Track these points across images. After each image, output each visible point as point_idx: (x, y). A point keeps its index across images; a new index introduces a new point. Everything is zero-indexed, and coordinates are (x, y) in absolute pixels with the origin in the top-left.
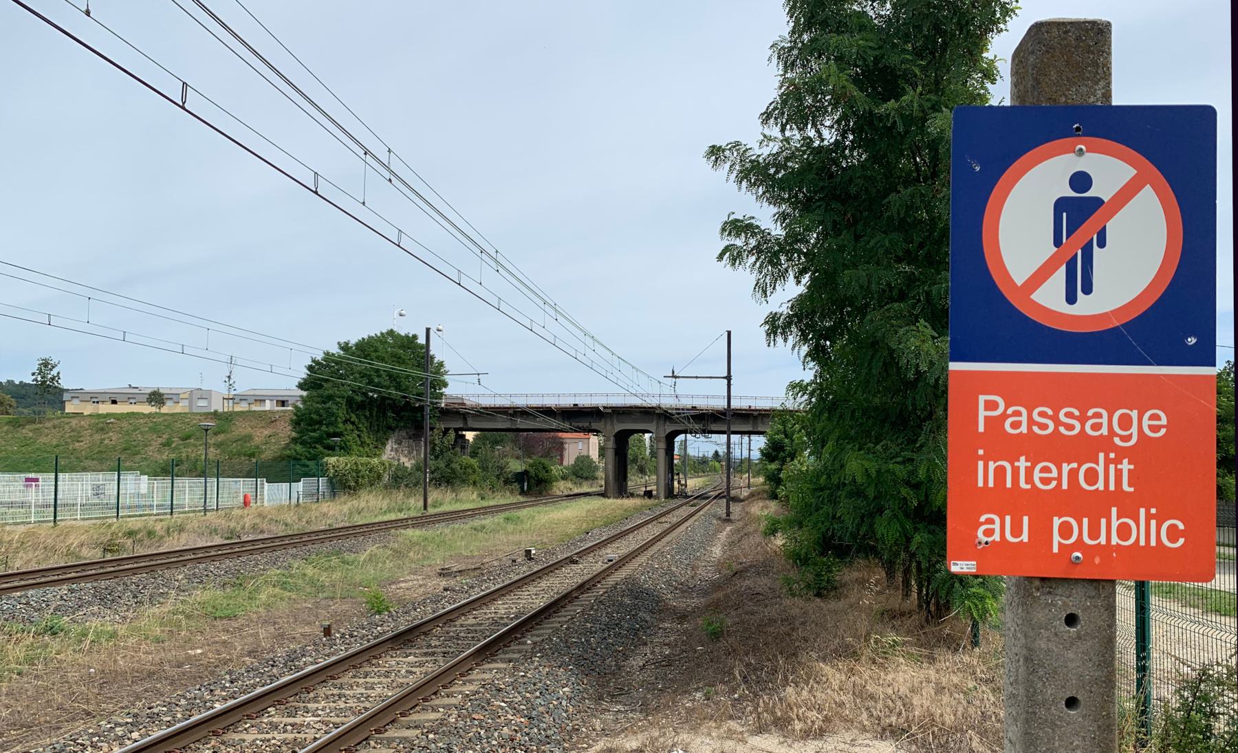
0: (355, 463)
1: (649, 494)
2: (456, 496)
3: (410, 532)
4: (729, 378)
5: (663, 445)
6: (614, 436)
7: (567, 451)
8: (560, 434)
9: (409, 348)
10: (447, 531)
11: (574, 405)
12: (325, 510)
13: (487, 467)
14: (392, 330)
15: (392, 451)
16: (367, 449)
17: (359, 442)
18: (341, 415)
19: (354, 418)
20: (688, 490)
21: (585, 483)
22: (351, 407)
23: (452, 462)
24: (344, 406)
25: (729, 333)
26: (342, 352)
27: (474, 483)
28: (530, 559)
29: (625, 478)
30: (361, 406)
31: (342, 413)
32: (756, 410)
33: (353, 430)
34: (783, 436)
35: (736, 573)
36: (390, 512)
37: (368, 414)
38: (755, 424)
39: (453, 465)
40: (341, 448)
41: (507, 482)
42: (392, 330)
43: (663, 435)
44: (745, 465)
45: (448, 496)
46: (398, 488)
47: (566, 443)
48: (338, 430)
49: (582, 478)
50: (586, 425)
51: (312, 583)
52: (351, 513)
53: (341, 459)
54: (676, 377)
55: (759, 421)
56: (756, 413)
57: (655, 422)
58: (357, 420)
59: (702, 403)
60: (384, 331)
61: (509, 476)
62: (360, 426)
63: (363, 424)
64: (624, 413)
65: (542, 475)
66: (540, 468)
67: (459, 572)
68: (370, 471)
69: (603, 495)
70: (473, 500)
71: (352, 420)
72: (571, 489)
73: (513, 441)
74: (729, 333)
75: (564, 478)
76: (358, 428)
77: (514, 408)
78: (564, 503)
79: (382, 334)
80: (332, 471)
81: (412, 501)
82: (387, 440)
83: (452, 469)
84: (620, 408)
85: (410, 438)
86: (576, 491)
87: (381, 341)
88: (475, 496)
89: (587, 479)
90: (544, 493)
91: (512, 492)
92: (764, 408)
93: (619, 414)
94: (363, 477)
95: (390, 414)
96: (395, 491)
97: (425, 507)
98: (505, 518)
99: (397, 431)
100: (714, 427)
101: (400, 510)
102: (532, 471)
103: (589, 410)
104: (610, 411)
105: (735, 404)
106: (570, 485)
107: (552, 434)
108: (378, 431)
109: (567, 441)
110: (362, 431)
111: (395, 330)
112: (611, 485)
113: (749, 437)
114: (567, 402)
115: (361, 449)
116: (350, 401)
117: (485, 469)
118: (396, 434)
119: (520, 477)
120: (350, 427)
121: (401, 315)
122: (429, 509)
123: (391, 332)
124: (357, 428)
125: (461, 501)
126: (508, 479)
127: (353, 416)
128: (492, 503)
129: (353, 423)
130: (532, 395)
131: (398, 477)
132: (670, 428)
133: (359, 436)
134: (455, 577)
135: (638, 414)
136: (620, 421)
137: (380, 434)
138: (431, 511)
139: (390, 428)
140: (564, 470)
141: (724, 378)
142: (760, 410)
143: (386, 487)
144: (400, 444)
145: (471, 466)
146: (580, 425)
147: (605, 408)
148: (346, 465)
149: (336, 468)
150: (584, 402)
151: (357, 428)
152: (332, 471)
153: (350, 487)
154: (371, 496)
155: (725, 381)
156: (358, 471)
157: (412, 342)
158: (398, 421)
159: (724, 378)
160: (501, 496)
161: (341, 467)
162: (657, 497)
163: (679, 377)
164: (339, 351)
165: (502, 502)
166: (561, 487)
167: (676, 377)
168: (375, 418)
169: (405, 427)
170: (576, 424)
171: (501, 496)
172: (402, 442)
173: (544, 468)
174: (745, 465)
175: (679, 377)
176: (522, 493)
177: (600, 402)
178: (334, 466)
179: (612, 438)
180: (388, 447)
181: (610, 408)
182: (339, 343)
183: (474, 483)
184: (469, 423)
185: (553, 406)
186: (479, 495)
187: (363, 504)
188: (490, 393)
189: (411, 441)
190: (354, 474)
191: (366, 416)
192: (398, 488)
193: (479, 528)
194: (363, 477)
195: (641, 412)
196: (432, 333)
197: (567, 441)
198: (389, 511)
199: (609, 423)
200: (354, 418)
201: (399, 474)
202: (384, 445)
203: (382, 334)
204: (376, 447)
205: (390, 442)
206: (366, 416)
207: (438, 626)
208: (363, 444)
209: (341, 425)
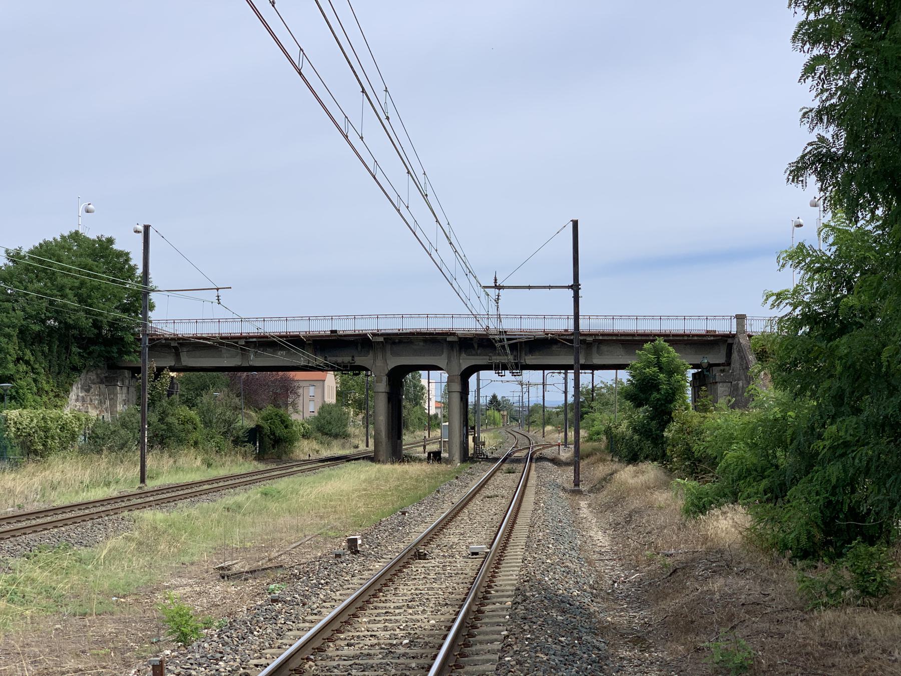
0: (43, 418)
1: (435, 457)
2: (175, 462)
3: (148, 515)
4: (575, 287)
5: (457, 387)
6: (387, 375)
7: (301, 398)
8: (292, 374)
9: (102, 257)
10: (194, 512)
11: (332, 331)
12: (10, 484)
13: (211, 422)
14: (77, 232)
15: (77, 400)
16: (45, 398)
17: (35, 389)
18: (12, 351)
19: (28, 355)
20: (487, 449)
21: (336, 443)
22: (25, 341)
23: (167, 415)
24: (15, 339)
25: (575, 224)
26: (11, 264)
27: (196, 443)
28: (356, 552)
29: (399, 436)
30: (38, 338)
31: (13, 348)
32: (591, 335)
33: (27, 373)
34: (656, 369)
35: (675, 571)
36: (94, 486)
37: (46, 349)
38: (588, 355)
39: (170, 419)
40: (12, 398)
41: (236, 442)
42: (77, 232)
43: (457, 372)
44: (537, 417)
45: (167, 462)
46: (100, 452)
47: (299, 387)
48: (7, 373)
49: (330, 435)
50: (347, 359)
51: (48, 592)
52: (44, 489)
53: (25, 412)
54: (499, 288)
55: (594, 349)
56: (590, 339)
57: (445, 356)
58: (32, 359)
59: (535, 326)
60: (66, 234)
61: (240, 433)
62: (37, 366)
63: (41, 364)
64: (400, 342)
65: (280, 431)
66: (277, 422)
67: (252, 572)
68: (62, 429)
69: (373, 458)
70: (198, 469)
71: (26, 358)
72: (317, 452)
73: (228, 386)
74: (575, 224)
75: (306, 436)
76: (33, 370)
77: (245, 338)
78: (327, 470)
79: (63, 237)
80: (13, 429)
81: (120, 471)
82: (71, 385)
83: (167, 424)
84: (396, 334)
85: (101, 382)
86: (326, 453)
87: (63, 248)
88: (199, 462)
89: (336, 436)
90: (284, 457)
91: (245, 455)
92: (674, 332)
93: (394, 343)
94: (53, 438)
95: (75, 349)
96: (96, 457)
97: (143, 480)
98: (262, 493)
99: (84, 371)
100: (530, 360)
101: (108, 484)
102: (266, 426)
103: (352, 339)
104: (381, 339)
105: (584, 326)
106: (315, 445)
107: (280, 373)
108: (59, 373)
109: (301, 384)
110: (38, 373)
111: (81, 231)
112: (384, 444)
113: (593, 374)
114: (322, 328)
115: (38, 398)
116: (23, 332)
117: (207, 424)
118: (83, 376)
119: (254, 434)
120: (23, 367)
121: (88, 212)
122: (147, 481)
123: (76, 236)
124: (33, 369)
125: (178, 469)
126: (238, 437)
127: (28, 352)
128: (222, 472)
129: (27, 363)
130: (294, 319)
131: (98, 437)
132: (467, 362)
133: (35, 381)
134: (246, 579)
135: (422, 344)
136: (395, 354)
137: (62, 378)
138: (151, 484)
139: (75, 369)
140: (306, 425)
141: (569, 287)
142: (596, 335)
143: (82, 451)
144: (88, 391)
145: (190, 421)
146: (340, 360)
147: (374, 335)
148: (32, 421)
149: (18, 426)
150: (345, 327)
151: (33, 369)
152: (13, 429)
153: (36, 452)
154: (67, 464)
155: (571, 292)
156: (46, 430)
157: (107, 248)
158: (86, 359)
159: (569, 287)
160: (232, 461)
161: (25, 422)
162: (448, 461)
163: (503, 287)
164: (7, 262)
165: (237, 470)
166: (305, 448)
167: (499, 288)
168: (55, 353)
169: (96, 366)
170: (334, 359)
171: (232, 461)
172: (90, 387)
173: (283, 422)
174: (537, 417)
175: (503, 287)
176: (260, 458)
177: (366, 326)
178: (15, 423)
179: (385, 379)
180: (73, 396)
181: (382, 335)
182: (7, 251)
183: (196, 443)
184: (183, 359)
185: (302, 334)
186: (204, 461)
187: (58, 476)
188: (230, 316)
189: (103, 386)
190: (42, 434)
191: (43, 352)
192: (100, 452)
193: (234, 507)
194: (53, 438)
195: (425, 341)
196: (152, 232)
197: (301, 384)
198: (94, 484)
199: (380, 357)
200: (28, 355)
201: (99, 431)
202: (67, 392)
203: (63, 237)
204: (57, 396)
205: (74, 388)
206: (43, 352)
207: (308, 659)
208: (40, 392)
209: (11, 365)
